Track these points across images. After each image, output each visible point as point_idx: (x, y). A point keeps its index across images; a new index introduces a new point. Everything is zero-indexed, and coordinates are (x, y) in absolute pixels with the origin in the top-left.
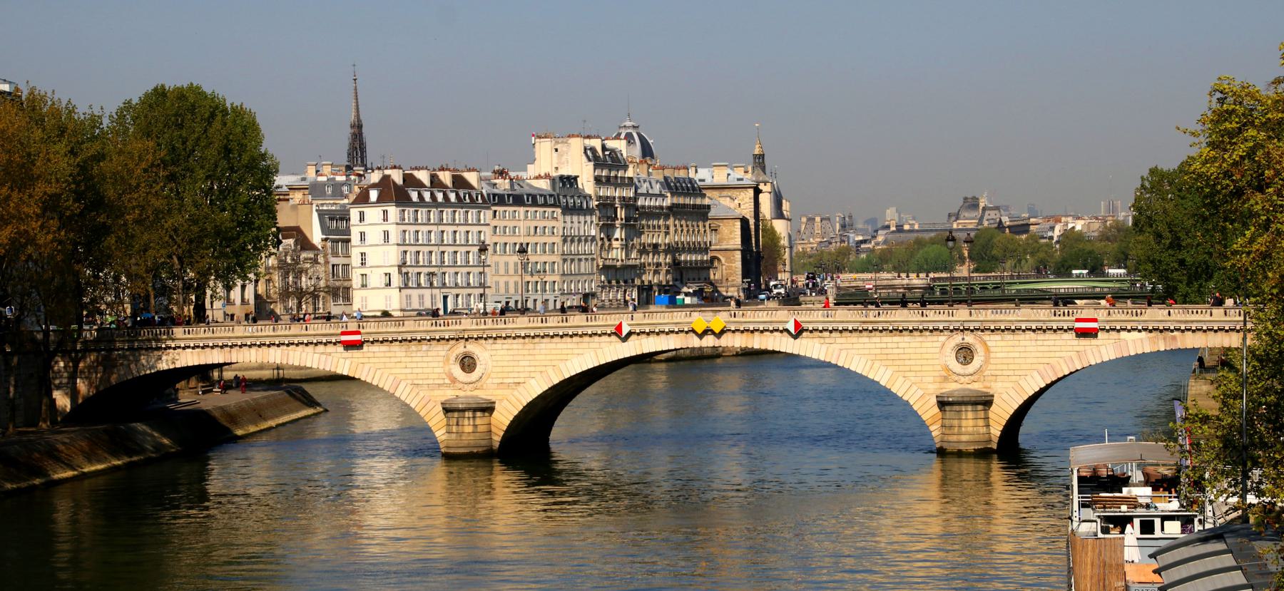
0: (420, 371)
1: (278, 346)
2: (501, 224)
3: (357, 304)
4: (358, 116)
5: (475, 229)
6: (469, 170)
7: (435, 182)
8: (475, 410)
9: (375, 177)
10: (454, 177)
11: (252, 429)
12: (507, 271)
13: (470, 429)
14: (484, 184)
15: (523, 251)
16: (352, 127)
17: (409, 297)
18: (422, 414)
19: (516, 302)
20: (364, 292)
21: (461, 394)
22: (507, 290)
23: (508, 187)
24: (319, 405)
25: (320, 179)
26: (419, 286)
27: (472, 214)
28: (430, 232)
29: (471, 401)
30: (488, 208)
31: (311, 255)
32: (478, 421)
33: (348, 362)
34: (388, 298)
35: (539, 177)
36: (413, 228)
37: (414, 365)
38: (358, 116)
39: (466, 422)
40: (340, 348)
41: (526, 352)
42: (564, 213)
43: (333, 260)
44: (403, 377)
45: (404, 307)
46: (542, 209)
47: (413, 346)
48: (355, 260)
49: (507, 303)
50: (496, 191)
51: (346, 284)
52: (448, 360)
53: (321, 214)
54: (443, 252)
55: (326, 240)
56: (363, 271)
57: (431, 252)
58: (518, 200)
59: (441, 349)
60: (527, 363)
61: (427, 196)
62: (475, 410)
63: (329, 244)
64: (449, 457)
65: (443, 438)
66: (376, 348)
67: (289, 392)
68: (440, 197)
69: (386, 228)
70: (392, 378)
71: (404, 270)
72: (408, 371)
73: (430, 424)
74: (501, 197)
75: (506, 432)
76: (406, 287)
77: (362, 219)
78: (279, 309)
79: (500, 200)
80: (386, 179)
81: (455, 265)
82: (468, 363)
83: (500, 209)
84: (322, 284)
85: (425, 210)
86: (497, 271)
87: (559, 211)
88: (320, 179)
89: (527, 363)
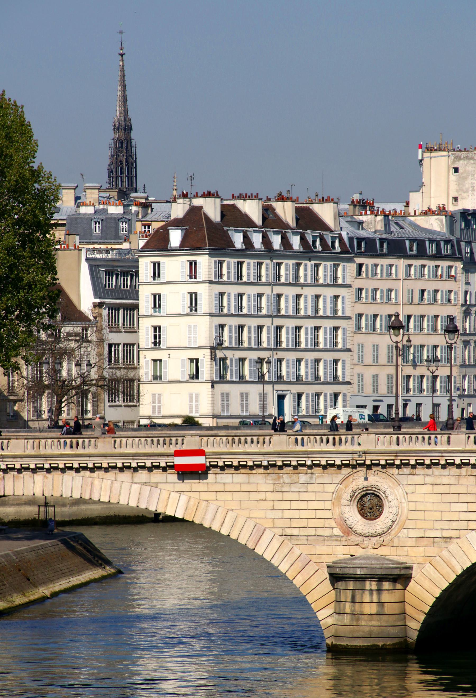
0: (295, 514)
1: (78, 470)
2: (369, 285)
3: (145, 408)
4: (125, 111)
5: (329, 292)
6: (323, 201)
7: (270, 219)
8: (381, 579)
9: (179, 210)
10: (298, 210)
11: (18, 600)
12: (376, 358)
13: (372, 609)
14: (344, 223)
15: (396, 326)
16: (116, 128)
17: (226, 396)
18: (298, 582)
19: (390, 407)
20: (156, 388)
21: (359, 552)
22: (375, 388)
23: (380, 227)
24: (108, 563)
25: (83, 210)
26: (242, 379)
27: (325, 269)
28: (260, 296)
29: (375, 564)
30: (350, 260)
31: (78, 329)
32: (386, 597)
33: (184, 498)
34: (194, 398)
35: (428, 213)
36: (234, 290)
37: (286, 505)
38: (125, 111)
39: (367, 598)
40: (172, 477)
41: (463, 489)
42: (466, 270)
43: (113, 338)
44: (268, 523)
45: (218, 411)
46: (431, 263)
47: (286, 476)
48: (145, 337)
49: (376, 408)
50: (362, 234)
51: (131, 374)
52: (339, 498)
53: (94, 266)
54: (279, 328)
55: (100, 305)
56: (157, 355)
57: (260, 328)
58: (396, 249)
59: (329, 482)
60: (464, 507)
61: (257, 240)
62: (381, 579)
63: (105, 312)
64: (337, 652)
65: (330, 621)
66: (227, 477)
67: (65, 543)
68: (276, 241)
69: (193, 288)
70: (251, 524)
71: (220, 354)
72: (278, 514)
73: (310, 599)
74: (370, 242)
75: (429, 615)
76: (222, 380)
77: (157, 273)
78: (26, 412)
79: (369, 247)
80: (195, 212)
81: (315, 347)
82: (370, 504)
83: (368, 262)
84: (94, 374)
85: (253, 262)
86: (361, 358)
87: (459, 265)
88: (83, 210)
89: (464, 507)
